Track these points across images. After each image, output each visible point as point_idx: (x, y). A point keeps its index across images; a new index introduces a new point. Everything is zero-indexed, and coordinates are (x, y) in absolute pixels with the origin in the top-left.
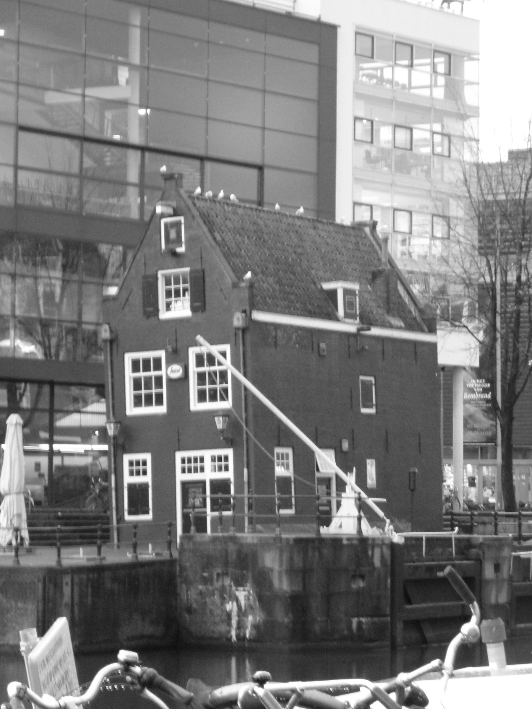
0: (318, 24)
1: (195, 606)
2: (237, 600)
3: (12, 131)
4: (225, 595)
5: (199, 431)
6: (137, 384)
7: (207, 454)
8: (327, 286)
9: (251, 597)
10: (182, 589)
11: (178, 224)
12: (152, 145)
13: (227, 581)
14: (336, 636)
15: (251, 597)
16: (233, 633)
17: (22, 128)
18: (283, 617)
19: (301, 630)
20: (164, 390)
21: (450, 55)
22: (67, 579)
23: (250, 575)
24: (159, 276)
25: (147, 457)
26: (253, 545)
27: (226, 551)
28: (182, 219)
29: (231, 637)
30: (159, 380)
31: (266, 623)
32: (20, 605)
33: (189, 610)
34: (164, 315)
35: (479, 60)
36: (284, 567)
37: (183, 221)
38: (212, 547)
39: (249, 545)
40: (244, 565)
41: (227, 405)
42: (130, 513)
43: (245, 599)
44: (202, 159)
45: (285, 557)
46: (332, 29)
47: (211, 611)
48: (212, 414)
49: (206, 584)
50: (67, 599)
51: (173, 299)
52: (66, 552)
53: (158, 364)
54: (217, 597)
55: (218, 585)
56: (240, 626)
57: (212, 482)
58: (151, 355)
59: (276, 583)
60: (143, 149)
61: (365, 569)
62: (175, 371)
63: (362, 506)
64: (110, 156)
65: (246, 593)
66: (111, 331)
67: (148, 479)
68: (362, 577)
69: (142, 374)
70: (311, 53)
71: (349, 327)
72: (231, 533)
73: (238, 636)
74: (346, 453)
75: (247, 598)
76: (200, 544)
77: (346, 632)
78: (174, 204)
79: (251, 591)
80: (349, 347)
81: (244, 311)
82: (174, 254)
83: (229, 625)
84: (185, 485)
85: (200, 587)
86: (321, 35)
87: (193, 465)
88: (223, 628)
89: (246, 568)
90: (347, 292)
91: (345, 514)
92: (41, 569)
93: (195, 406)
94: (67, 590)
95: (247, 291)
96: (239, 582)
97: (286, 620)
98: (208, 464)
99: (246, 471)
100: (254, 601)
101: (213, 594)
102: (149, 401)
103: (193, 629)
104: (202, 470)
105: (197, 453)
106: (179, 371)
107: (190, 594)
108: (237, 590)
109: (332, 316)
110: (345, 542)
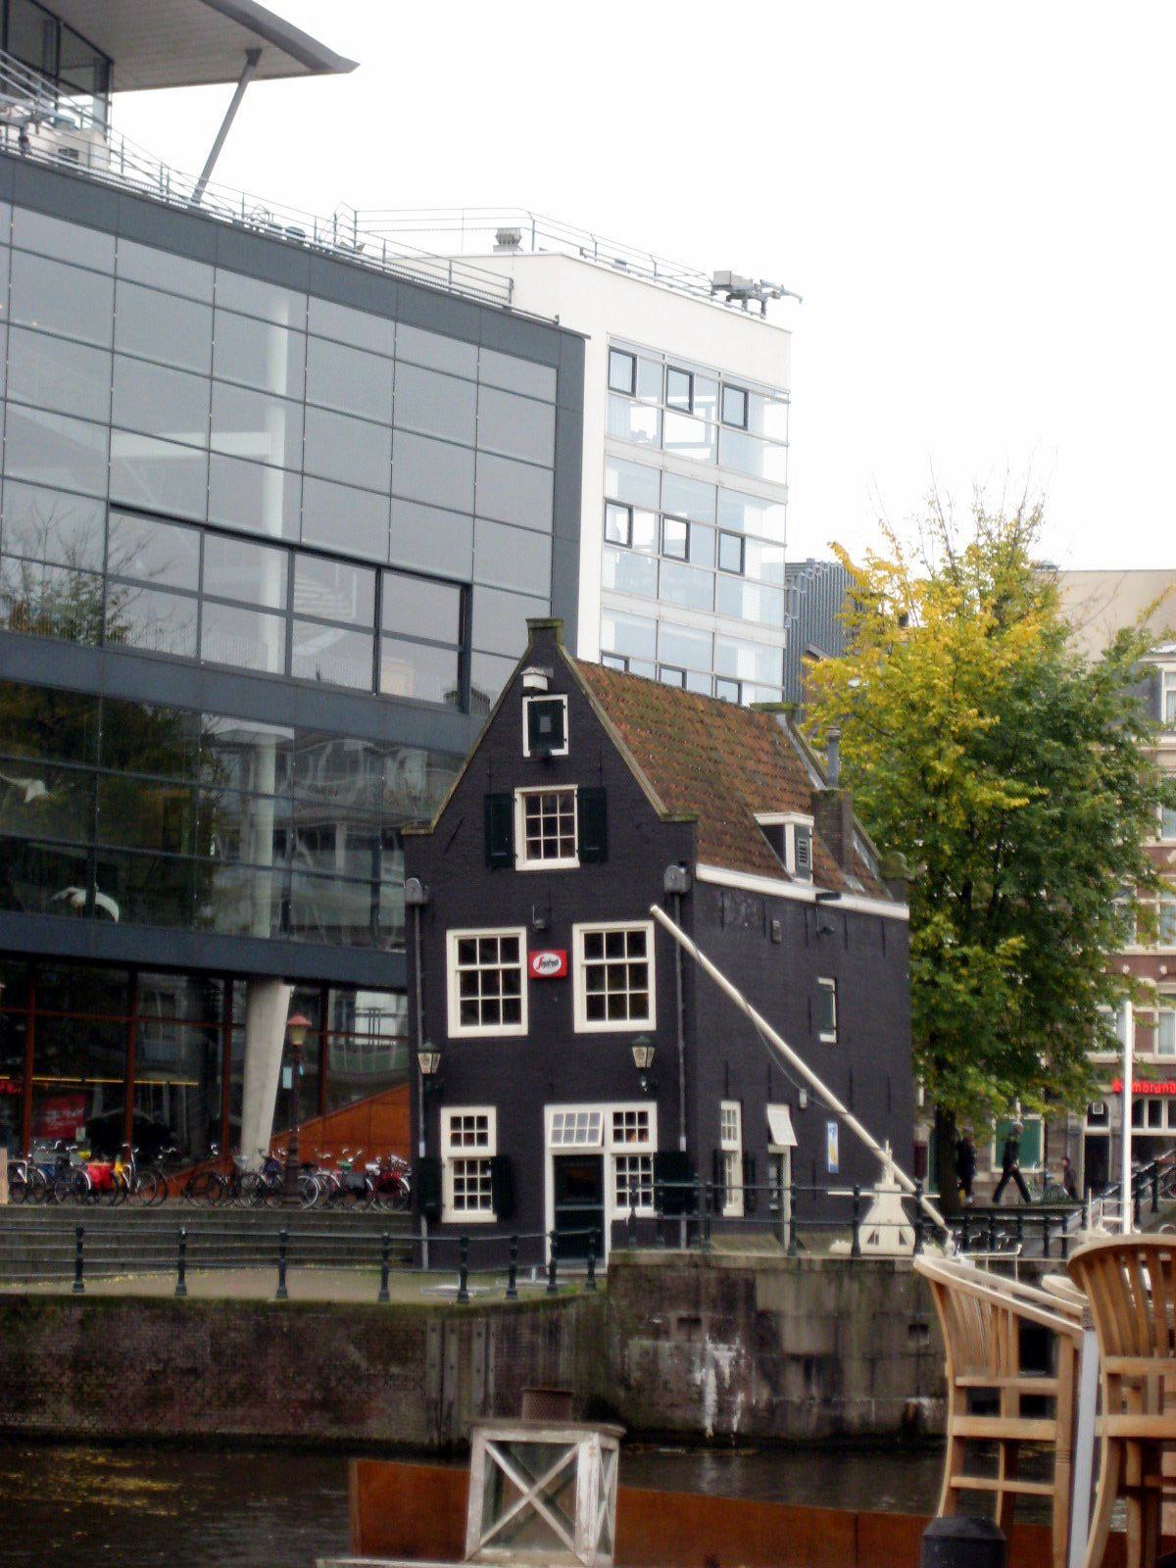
0: (553, 329)
2: (717, 1365)
3: (100, 508)
5: (601, 1072)
6: (468, 982)
8: (765, 819)
9: (742, 1362)
12: (306, 541)
15: (742, 1362)
20: (524, 996)
23: (741, 1320)
24: (517, 796)
25: (490, 1113)
27: (698, 1279)
28: (564, 698)
29: (704, 1430)
30: (512, 980)
35: (787, 402)
37: (565, 703)
40: (735, 1305)
41: (649, 1024)
43: (731, 1365)
44: (379, 568)
48: (630, 1038)
52: (294, 1275)
53: (510, 948)
56: (724, 1408)
58: (498, 933)
62: (548, 963)
63: (912, 1207)
65: (732, 1354)
70: (542, 380)
71: (803, 890)
74: (800, 1109)
79: (743, 1351)
80: (806, 926)
86: (556, 347)
90: (800, 830)
93: (582, 1024)
100: (749, 1366)
102: (490, 1014)
106: (555, 963)
108: (717, 1349)
109: (778, 872)
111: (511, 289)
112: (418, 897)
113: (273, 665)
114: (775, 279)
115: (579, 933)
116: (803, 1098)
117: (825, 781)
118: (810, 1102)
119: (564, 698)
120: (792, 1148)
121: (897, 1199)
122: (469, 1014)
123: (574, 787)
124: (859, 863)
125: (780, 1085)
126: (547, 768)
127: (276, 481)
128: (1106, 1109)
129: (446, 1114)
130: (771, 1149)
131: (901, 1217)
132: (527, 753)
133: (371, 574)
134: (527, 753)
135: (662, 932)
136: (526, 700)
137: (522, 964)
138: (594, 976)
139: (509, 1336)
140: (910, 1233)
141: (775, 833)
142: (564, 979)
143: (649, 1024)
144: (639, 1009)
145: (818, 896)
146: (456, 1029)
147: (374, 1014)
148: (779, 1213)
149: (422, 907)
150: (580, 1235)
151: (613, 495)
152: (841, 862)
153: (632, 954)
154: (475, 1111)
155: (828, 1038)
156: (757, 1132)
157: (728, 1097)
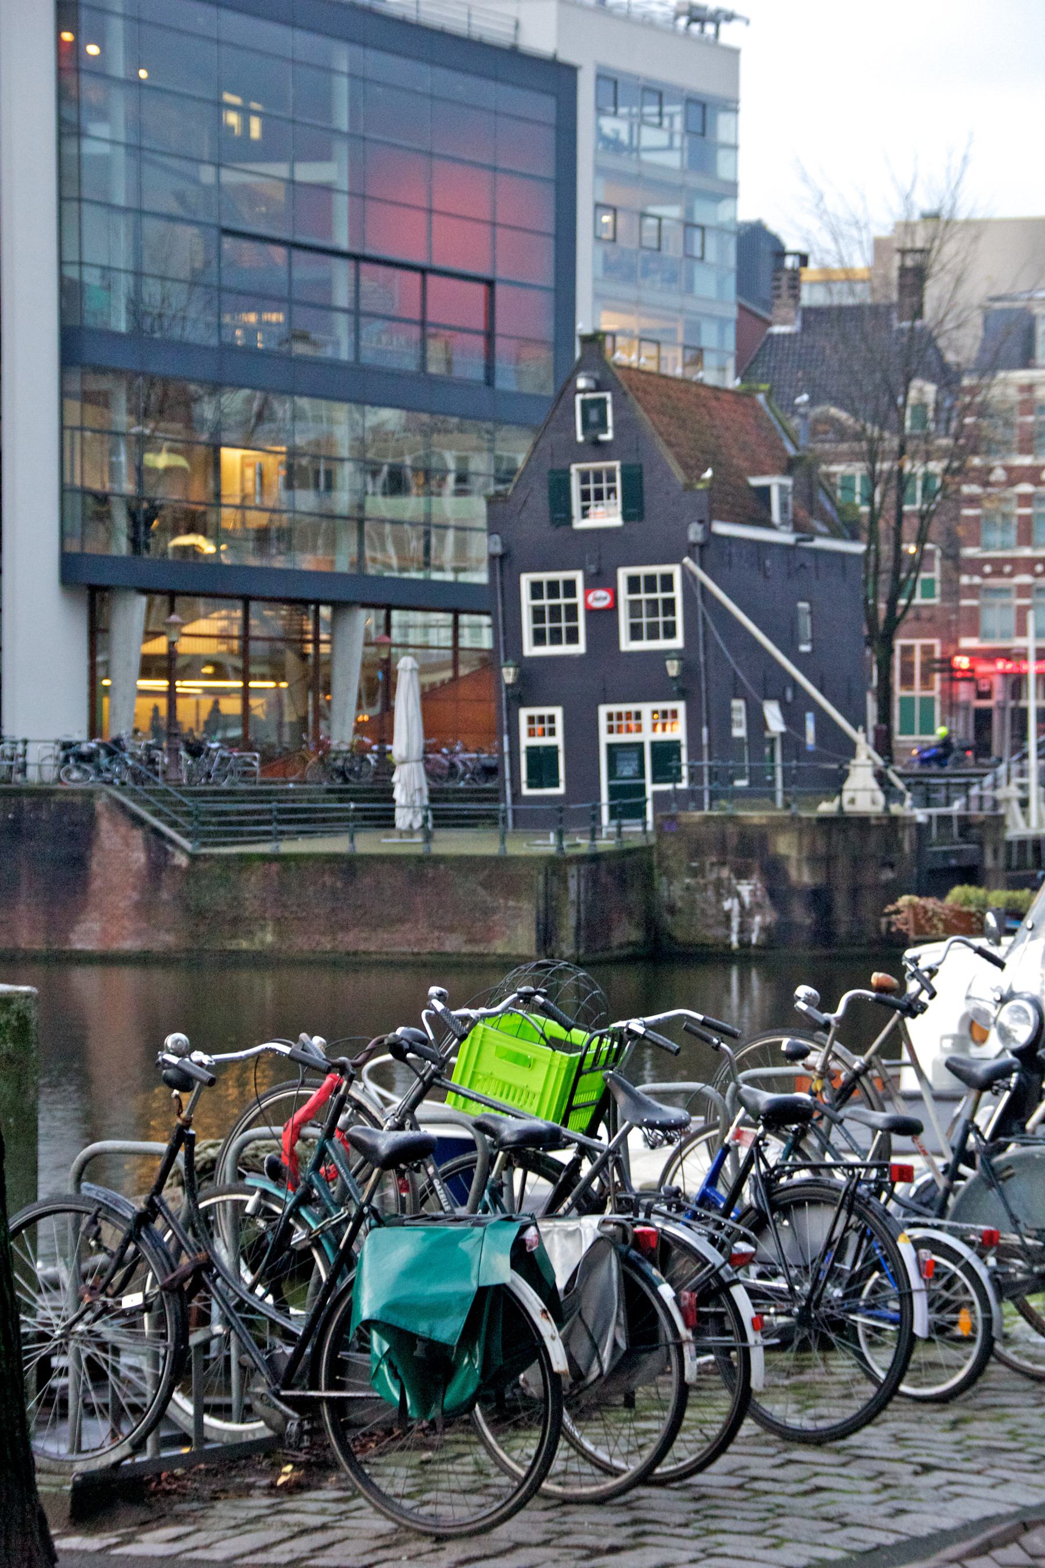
1: (679, 904)
2: (738, 895)
3: (214, 232)
4: (723, 889)
5: (645, 680)
6: (538, 614)
7: (646, 709)
8: (755, 481)
10: (661, 884)
11: (602, 402)
13: (725, 873)
14: (864, 941)
16: (734, 939)
17: (227, 232)
18: (802, 916)
19: (824, 933)
21: (704, 106)
22: (572, 870)
23: (756, 865)
25: (558, 712)
26: (762, 826)
28: (608, 396)
30: (572, 611)
31: (779, 924)
32: (511, 903)
33: (672, 910)
34: (579, 524)
36: (805, 854)
38: (703, 829)
39: (756, 826)
40: (749, 851)
41: (678, 642)
42: (530, 786)
44: (424, 271)
45: (806, 841)
46: (571, 71)
47: (703, 911)
48: (663, 655)
49: (695, 876)
50: (573, 896)
51: (592, 502)
53: (570, 588)
54: (710, 893)
55: (712, 876)
56: (744, 929)
57: (654, 744)
58: (560, 576)
59: (793, 873)
60: (357, 258)
61: (895, 856)
62: (600, 599)
64: (306, 267)
66: (503, 545)
67: (558, 740)
68: (892, 866)
69: (546, 602)
70: (545, 107)
71: (785, 537)
72: (673, 812)
73: (740, 941)
75: (753, 893)
76: (687, 825)
77: (874, 936)
78: (597, 375)
81: (701, 522)
82: (597, 443)
83: (728, 927)
84: (610, 747)
85: (687, 880)
86: (556, 76)
87: (624, 722)
88: (720, 932)
89: (751, 855)
90: (782, 488)
91: (860, 786)
92: (541, 858)
93: (627, 644)
94: (572, 884)
95: (705, 495)
96: (742, 874)
97: (808, 921)
98: (647, 720)
99: (705, 731)
101: (705, 888)
102: (556, 638)
103: (679, 934)
104: (639, 729)
105: (632, 707)
107: (672, 890)
109: (766, 523)
110: (873, 822)
111: (517, 26)
112: (498, 549)
113: (345, 354)
114: (728, 6)
115: (623, 574)
116: (789, 695)
117: (797, 448)
118: (795, 697)
119: (608, 396)
120: (782, 734)
121: (869, 772)
122: (539, 638)
123: (617, 464)
124: (822, 509)
125: (773, 684)
126: (597, 448)
127: (342, 205)
128: (991, 685)
129: (524, 713)
130: (767, 735)
131: (873, 784)
132: (580, 438)
133: (417, 277)
134: (580, 438)
135: (687, 575)
136: (579, 398)
137: (579, 599)
138: (635, 607)
139: (594, 880)
140: (880, 797)
141: (764, 492)
142: (613, 608)
143: (678, 642)
144: (670, 632)
145: (798, 540)
146: (530, 650)
147: (406, 627)
148: (772, 783)
149: (502, 557)
150: (628, 801)
151: (602, 200)
152: (811, 513)
153: (663, 590)
154: (546, 711)
155: (805, 648)
156: (757, 721)
157: (736, 697)
